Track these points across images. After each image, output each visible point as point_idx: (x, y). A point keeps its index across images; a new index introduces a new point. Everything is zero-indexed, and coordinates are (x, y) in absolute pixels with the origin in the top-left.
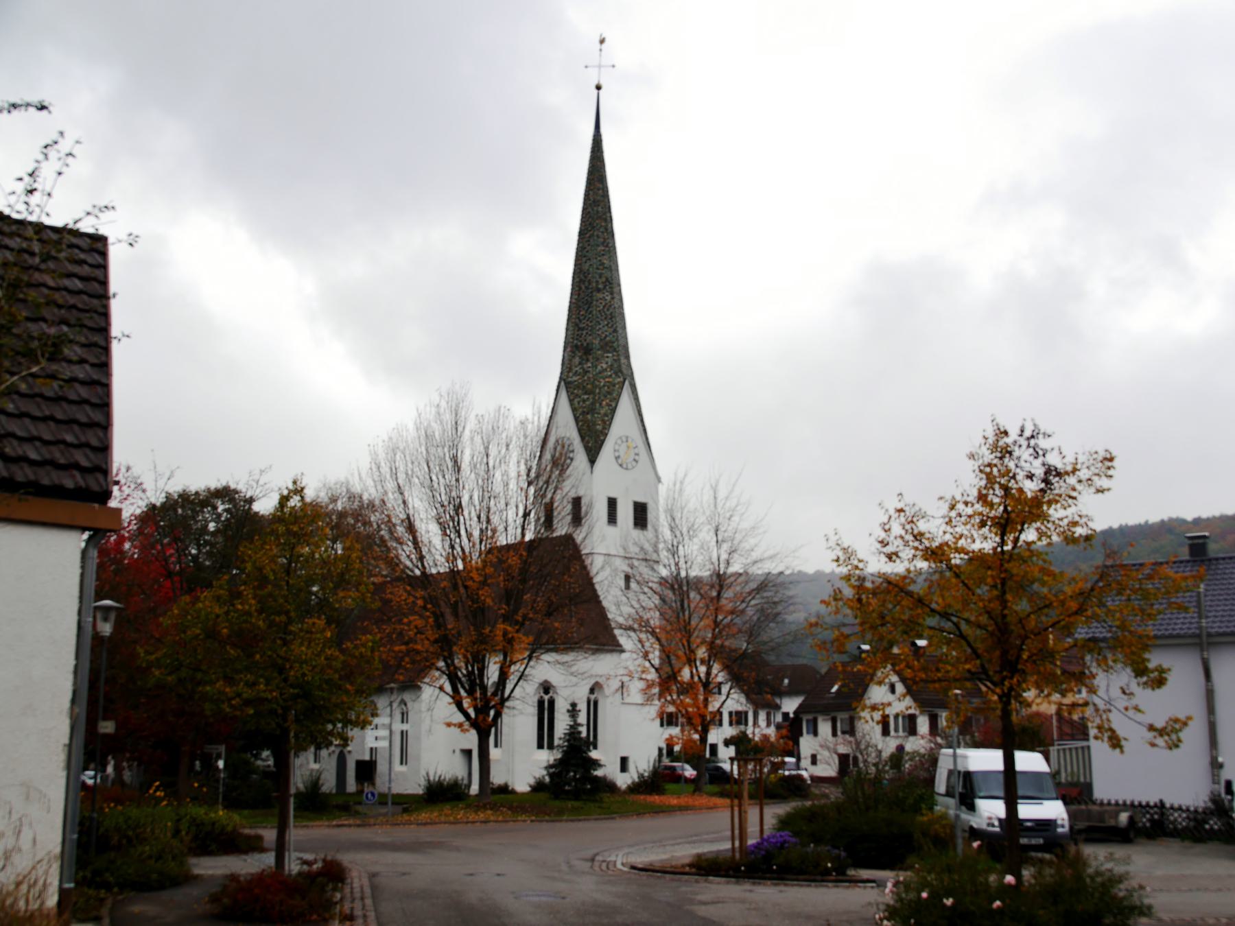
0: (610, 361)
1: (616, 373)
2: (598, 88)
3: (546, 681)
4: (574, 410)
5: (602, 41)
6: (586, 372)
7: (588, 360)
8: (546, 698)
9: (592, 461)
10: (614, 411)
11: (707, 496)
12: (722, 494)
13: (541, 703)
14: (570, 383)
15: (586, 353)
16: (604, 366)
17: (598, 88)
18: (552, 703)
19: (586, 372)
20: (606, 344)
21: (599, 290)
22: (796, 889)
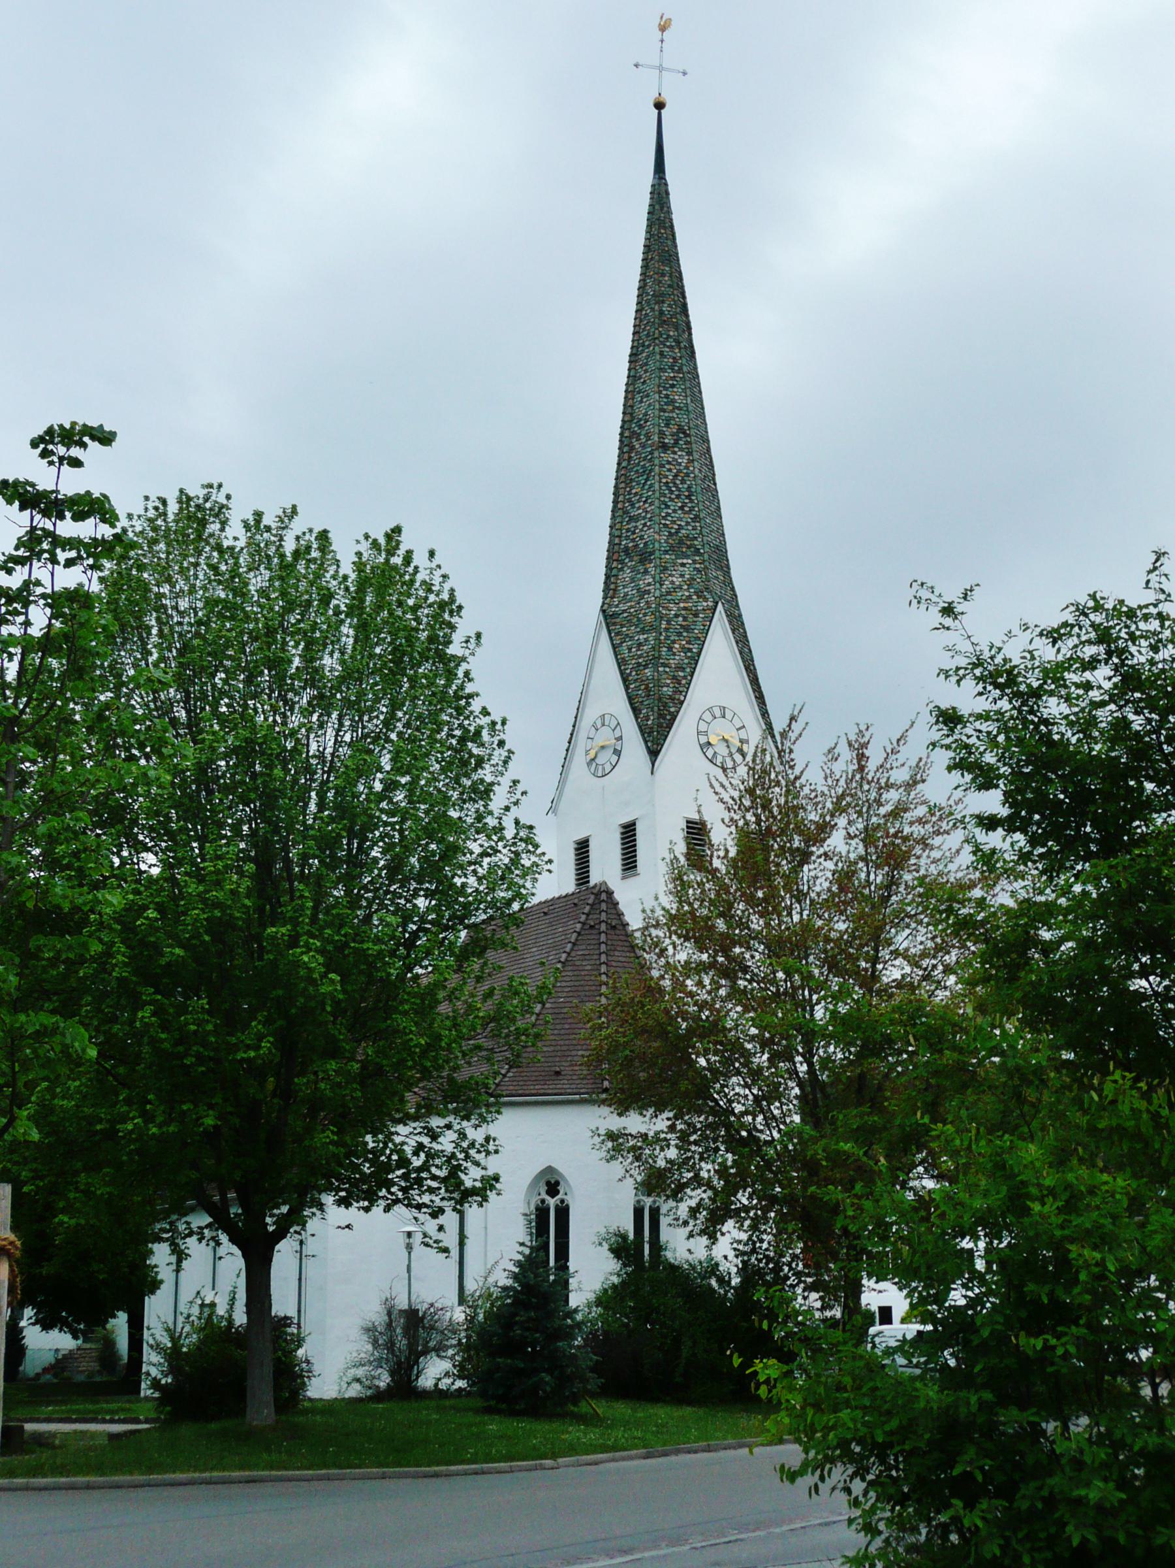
0: (687, 572)
1: (699, 594)
2: (659, 106)
3: (550, 1170)
4: (621, 663)
5: (685, 74)
6: (643, 593)
7: (646, 572)
8: (552, 1202)
9: (654, 754)
10: (695, 660)
11: (845, 764)
12: (875, 757)
13: (542, 1213)
14: (615, 615)
15: (642, 562)
16: (677, 581)
17: (659, 106)
18: (563, 1213)
19: (643, 593)
20: (681, 542)
21: (664, 447)
22: (632, 1469)
